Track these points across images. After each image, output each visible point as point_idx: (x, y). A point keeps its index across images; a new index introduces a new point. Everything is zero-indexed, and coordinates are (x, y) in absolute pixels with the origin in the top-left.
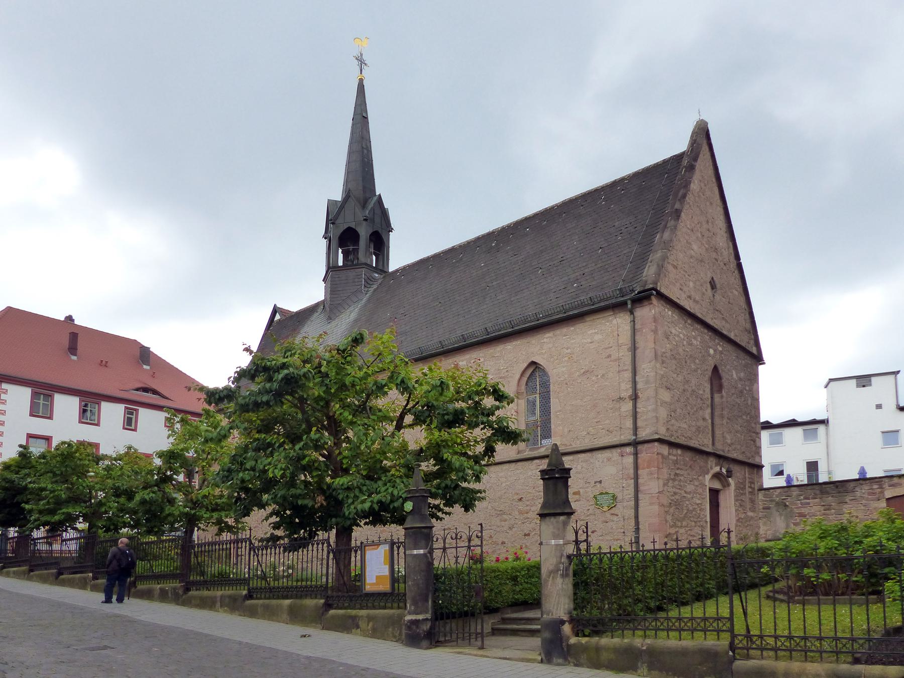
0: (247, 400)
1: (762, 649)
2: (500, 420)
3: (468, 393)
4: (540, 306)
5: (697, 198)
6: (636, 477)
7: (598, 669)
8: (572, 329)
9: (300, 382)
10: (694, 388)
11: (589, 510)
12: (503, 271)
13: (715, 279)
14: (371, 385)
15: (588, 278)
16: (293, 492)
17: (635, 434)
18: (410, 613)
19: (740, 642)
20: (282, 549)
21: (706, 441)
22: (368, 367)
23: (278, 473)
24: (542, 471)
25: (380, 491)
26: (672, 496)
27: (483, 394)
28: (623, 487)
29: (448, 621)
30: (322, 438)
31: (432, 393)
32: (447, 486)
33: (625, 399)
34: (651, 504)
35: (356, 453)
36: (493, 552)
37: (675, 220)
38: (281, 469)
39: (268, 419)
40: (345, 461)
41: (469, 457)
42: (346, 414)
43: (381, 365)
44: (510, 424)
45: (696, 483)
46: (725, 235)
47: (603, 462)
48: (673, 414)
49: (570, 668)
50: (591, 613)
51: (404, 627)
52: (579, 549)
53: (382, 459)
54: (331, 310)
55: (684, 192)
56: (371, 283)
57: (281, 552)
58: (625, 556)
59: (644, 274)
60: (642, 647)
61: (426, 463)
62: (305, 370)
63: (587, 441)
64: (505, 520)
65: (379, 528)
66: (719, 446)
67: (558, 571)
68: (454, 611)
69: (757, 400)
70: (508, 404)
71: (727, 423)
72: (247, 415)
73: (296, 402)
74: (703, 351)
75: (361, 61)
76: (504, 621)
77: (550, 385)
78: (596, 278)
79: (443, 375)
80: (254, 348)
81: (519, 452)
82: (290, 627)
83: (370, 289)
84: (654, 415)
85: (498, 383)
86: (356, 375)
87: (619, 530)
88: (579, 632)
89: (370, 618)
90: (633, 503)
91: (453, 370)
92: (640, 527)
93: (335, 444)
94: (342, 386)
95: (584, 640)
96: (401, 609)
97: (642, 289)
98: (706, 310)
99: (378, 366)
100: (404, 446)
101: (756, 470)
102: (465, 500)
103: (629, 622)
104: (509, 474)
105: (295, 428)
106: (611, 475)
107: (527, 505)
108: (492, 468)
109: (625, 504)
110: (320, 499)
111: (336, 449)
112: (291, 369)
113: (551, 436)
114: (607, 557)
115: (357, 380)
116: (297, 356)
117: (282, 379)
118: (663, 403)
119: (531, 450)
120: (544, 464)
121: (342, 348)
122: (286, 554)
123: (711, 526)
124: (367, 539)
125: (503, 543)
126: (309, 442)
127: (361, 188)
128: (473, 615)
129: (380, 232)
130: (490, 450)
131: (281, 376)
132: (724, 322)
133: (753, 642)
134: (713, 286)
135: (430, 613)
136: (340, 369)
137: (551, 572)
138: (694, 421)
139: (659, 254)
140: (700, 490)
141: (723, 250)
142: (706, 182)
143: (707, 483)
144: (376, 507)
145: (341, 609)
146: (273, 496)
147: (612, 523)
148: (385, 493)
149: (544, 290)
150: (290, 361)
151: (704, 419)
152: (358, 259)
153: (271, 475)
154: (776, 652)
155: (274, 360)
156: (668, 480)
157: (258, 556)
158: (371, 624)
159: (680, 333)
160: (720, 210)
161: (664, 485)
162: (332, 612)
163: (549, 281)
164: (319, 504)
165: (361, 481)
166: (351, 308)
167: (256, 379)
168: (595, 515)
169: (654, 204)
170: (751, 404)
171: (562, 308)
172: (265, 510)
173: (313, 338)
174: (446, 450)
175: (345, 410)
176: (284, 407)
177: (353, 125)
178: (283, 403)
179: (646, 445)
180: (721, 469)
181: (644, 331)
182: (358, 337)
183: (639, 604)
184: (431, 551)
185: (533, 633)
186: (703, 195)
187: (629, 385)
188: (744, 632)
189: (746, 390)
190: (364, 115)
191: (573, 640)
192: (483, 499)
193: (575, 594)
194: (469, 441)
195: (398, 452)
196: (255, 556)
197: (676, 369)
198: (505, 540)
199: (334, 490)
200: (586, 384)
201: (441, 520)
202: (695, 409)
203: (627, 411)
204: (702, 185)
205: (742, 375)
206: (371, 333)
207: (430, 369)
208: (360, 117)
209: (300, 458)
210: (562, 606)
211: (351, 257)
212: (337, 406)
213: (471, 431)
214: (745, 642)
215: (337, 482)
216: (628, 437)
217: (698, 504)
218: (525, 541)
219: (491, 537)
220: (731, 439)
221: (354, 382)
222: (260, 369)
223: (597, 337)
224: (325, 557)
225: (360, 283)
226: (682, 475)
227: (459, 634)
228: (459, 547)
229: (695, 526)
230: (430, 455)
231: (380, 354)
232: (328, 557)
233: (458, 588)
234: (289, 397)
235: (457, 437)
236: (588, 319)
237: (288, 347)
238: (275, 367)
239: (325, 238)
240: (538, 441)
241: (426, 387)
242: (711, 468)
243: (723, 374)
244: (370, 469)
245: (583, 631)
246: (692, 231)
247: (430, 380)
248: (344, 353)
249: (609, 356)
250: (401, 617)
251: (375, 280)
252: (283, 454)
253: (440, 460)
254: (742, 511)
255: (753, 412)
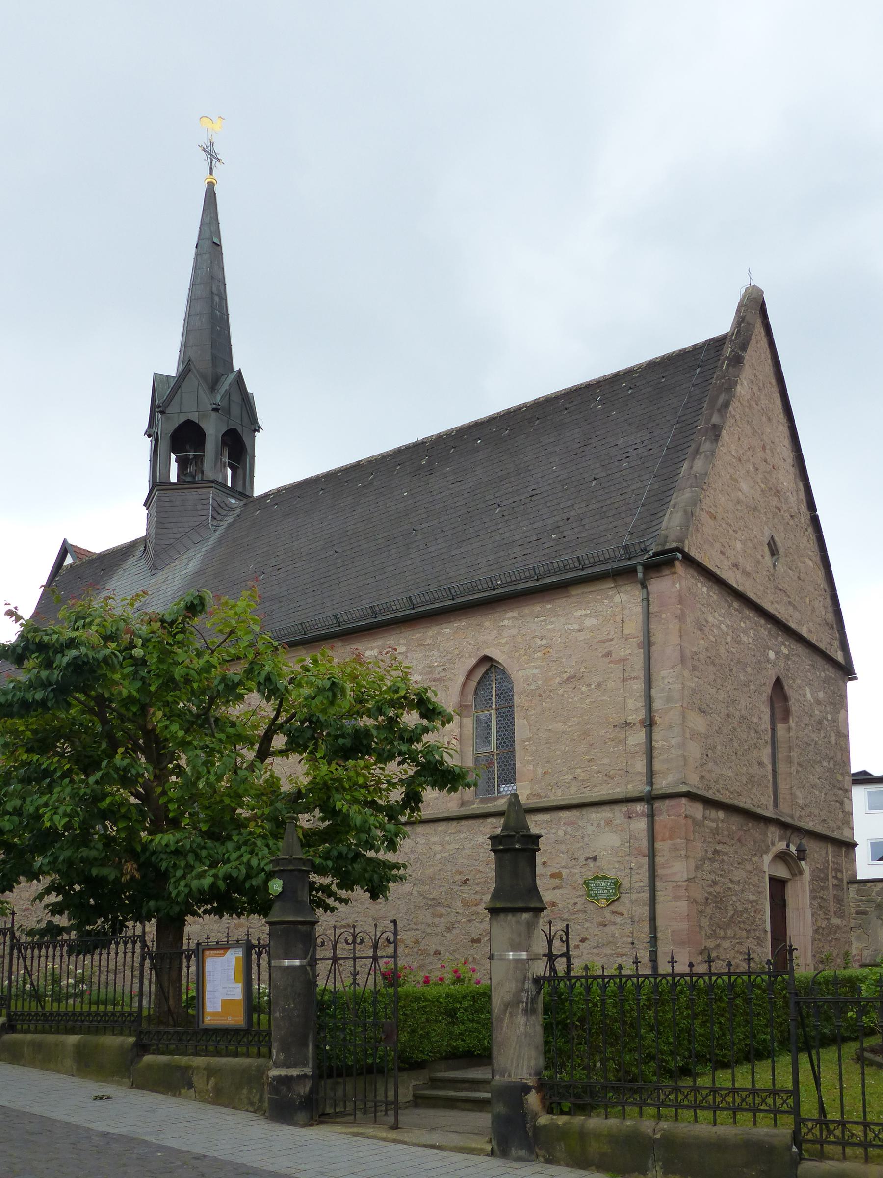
0: (10, 697)
1: (844, 1144)
2: (429, 750)
3: (377, 702)
4: (497, 566)
5: (747, 410)
6: (652, 854)
7: (584, 1168)
8: (549, 606)
9: (100, 672)
10: (743, 712)
11: (575, 904)
12: (437, 506)
13: (776, 539)
14: (216, 682)
15: (574, 525)
16: (85, 854)
17: (651, 783)
18: (277, 1065)
19: (810, 1131)
20: (65, 948)
21: (764, 800)
22: (213, 652)
23: (60, 822)
24: (493, 839)
25: (228, 858)
26: (711, 886)
27: (402, 707)
28: (631, 869)
29: (340, 1080)
30: (133, 767)
31: (317, 701)
32: (340, 854)
33: (634, 724)
34: (676, 898)
35: (191, 795)
36: (421, 967)
37: (712, 442)
38: (65, 815)
39: (45, 730)
40: (172, 807)
41: (378, 809)
42: (174, 728)
43: (232, 651)
44: (446, 757)
45: (749, 867)
46: (792, 470)
47: (599, 826)
48: (710, 753)
49: (537, 1167)
50: (572, 1076)
51: (266, 1088)
52: (553, 969)
53: (233, 805)
54: (156, 555)
55: (727, 397)
56: (224, 513)
57: (65, 954)
58: (626, 983)
59: (664, 525)
60: (655, 1134)
61: (306, 816)
62: (107, 652)
63: (573, 790)
64: (441, 916)
65: (228, 921)
66: (784, 807)
67: (519, 1004)
68: (349, 1063)
69: (846, 737)
70: (443, 725)
71: (797, 771)
72: (10, 721)
73: (92, 704)
74: (758, 654)
75: (211, 155)
76: (435, 1083)
77: (513, 695)
78: (587, 527)
79: (336, 671)
80: (27, 611)
81: (463, 804)
82: (77, 1080)
83: (222, 523)
84: (681, 752)
85: (426, 689)
86: (191, 666)
87: (625, 939)
88: (554, 1106)
89: (211, 1072)
90: (647, 895)
91: (353, 665)
92: (659, 935)
93: (155, 776)
94: (168, 681)
95: (561, 1120)
96: (264, 1057)
97: (660, 548)
98: (762, 588)
99: (227, 652)
100: (273, 783)
101: (844, 849)
102: (371, 880)
103: (634, 1091)
104: (447, 838)
105: (91, 747)
106: (612, 848)
107: (476, 893)
108: (420, 829)
109: (634, 897)
110: (130, 868)
111: (157, 786)
112: (83, 650)
113: (515, 780)
114: (598, 983)
115: (192, 672)
116: (94, 628)
117: (68, 664)
118: (695, 735)
119: (483, 801)
120: (496, 826)
121: (168, 618)
122: (73, 958)
123: (773, 939)
124: (208, 939)
125: (437, 953)
126: (112, 772)
127: (208, 357)
128: (381, 1071)
129: (240, 431)
130: (413, 799)
131: (65, 660)
132: (791, 608)
133: (830, 1132)
134: (773, 550)
135: (311, 1065)
136: (165, 654)
137: (507, 1005)
138: (745, 765)
139: (687, 495)
140: (755, 879)
141: (789, 494)
142: (761, 385)
143: (766, 868)
144: (222, 885)
145: (163, 1054)
146: (51, 859)
147: (613, 928)
148: (238, 863)
149: (505, 542)
150: (81, 636)
151: (760, 764)
152: (202, 472)
153: (48, 824)
154: (866, 1149)
155: (55, 632)
156: (703, 860)
157: (25, 959)
158: (212, 1081)
159: (721, 622)
160: (784, 429)
161: (697, 868)
162: (148, 1058)
163: (512, 527)
164: (128, 877)
165: (199, 840)
166: (191, 553)
167: (26, 662)
168: (585, 912)
169: (679, 414)
170: (836, 743)
171: (532, 572)
172: (39, 881)
173: (123, 600)
174: (339, 796)
175: (172, 721)
176: (72, 711)
177: (197, 255)
178: (69, 705)
179: (667, 802)
180: (788, 846)
181: (664, 616)
182: (195, 602)
183: (652, 1064)
184: (313, 963)
185: (480, 1105)
186: (757, 405)
187: (641, 703)
188: (816, 1115)
189: (827, 720)
190: (216, 240)
191: (544, 1119)
192: (401, 879)
193: (547, 1043)
194: (379, 782)
195: (263, 794)
196: (21, 960)
197: (715, 680)
198: (439, 948)
199: (154, 853)
200: (572, 698)
201: (332, 912)
202: (746, 747)
203: (636, 745)
204: (755, 389)
205: (821, 695)
206: (217, 597)
207: (315, 661)
208: (208, 243)
209: (97, 798)
210: (526, 1063)
211: (191, 469)
212: (160, 714)
213: (382, 766)
214: (817, 1131)
215: (156, 842)
216: (637, 786)
217: (751, 902)
218: (472, 952)
219: (417, 942)
220: (805, 798)
221: (187, 675)
222: (32, 647)
223: (590, 622)
224: (137, 965)
225: (205, 513)
226: (727, 853)
227: (358, 1103)
228: (359, 958)
229: (748, 938)
230: (314, 803)
231: (232, 632)
232: (142, 965)
233: (356, 1025)
234: (81, 697)
235: (358, 774)
236: (575, 591)
237: (79, 612)
238: (56, 645)
239: (149, 436)
240: (494, 786)
241: (306, 691)
242: (773, 844)
243: (790, 692)
244: (214, 821)
245: (559, 1104)
246: (740, 460)
247: (313, 679)
248: (172, 627)
249: (608, 654)
250: (261, 1072)
251: (231, 508)
252: (68, 790)
253: (330, 812)
254: (823, 916)
255: (839, 754)
